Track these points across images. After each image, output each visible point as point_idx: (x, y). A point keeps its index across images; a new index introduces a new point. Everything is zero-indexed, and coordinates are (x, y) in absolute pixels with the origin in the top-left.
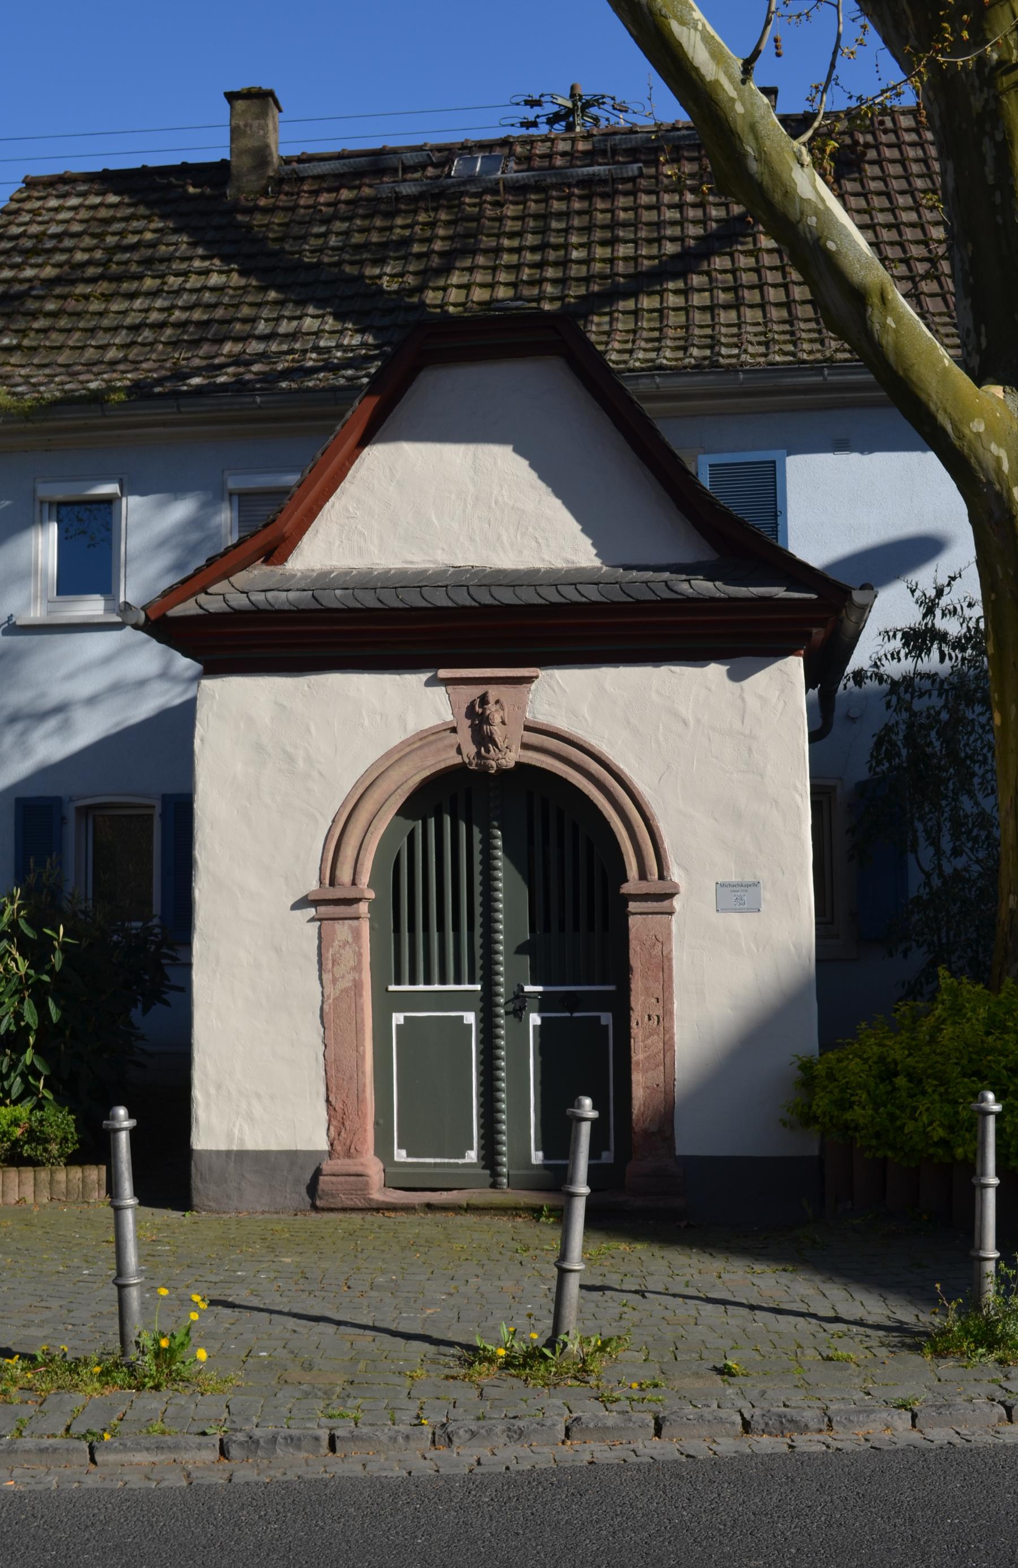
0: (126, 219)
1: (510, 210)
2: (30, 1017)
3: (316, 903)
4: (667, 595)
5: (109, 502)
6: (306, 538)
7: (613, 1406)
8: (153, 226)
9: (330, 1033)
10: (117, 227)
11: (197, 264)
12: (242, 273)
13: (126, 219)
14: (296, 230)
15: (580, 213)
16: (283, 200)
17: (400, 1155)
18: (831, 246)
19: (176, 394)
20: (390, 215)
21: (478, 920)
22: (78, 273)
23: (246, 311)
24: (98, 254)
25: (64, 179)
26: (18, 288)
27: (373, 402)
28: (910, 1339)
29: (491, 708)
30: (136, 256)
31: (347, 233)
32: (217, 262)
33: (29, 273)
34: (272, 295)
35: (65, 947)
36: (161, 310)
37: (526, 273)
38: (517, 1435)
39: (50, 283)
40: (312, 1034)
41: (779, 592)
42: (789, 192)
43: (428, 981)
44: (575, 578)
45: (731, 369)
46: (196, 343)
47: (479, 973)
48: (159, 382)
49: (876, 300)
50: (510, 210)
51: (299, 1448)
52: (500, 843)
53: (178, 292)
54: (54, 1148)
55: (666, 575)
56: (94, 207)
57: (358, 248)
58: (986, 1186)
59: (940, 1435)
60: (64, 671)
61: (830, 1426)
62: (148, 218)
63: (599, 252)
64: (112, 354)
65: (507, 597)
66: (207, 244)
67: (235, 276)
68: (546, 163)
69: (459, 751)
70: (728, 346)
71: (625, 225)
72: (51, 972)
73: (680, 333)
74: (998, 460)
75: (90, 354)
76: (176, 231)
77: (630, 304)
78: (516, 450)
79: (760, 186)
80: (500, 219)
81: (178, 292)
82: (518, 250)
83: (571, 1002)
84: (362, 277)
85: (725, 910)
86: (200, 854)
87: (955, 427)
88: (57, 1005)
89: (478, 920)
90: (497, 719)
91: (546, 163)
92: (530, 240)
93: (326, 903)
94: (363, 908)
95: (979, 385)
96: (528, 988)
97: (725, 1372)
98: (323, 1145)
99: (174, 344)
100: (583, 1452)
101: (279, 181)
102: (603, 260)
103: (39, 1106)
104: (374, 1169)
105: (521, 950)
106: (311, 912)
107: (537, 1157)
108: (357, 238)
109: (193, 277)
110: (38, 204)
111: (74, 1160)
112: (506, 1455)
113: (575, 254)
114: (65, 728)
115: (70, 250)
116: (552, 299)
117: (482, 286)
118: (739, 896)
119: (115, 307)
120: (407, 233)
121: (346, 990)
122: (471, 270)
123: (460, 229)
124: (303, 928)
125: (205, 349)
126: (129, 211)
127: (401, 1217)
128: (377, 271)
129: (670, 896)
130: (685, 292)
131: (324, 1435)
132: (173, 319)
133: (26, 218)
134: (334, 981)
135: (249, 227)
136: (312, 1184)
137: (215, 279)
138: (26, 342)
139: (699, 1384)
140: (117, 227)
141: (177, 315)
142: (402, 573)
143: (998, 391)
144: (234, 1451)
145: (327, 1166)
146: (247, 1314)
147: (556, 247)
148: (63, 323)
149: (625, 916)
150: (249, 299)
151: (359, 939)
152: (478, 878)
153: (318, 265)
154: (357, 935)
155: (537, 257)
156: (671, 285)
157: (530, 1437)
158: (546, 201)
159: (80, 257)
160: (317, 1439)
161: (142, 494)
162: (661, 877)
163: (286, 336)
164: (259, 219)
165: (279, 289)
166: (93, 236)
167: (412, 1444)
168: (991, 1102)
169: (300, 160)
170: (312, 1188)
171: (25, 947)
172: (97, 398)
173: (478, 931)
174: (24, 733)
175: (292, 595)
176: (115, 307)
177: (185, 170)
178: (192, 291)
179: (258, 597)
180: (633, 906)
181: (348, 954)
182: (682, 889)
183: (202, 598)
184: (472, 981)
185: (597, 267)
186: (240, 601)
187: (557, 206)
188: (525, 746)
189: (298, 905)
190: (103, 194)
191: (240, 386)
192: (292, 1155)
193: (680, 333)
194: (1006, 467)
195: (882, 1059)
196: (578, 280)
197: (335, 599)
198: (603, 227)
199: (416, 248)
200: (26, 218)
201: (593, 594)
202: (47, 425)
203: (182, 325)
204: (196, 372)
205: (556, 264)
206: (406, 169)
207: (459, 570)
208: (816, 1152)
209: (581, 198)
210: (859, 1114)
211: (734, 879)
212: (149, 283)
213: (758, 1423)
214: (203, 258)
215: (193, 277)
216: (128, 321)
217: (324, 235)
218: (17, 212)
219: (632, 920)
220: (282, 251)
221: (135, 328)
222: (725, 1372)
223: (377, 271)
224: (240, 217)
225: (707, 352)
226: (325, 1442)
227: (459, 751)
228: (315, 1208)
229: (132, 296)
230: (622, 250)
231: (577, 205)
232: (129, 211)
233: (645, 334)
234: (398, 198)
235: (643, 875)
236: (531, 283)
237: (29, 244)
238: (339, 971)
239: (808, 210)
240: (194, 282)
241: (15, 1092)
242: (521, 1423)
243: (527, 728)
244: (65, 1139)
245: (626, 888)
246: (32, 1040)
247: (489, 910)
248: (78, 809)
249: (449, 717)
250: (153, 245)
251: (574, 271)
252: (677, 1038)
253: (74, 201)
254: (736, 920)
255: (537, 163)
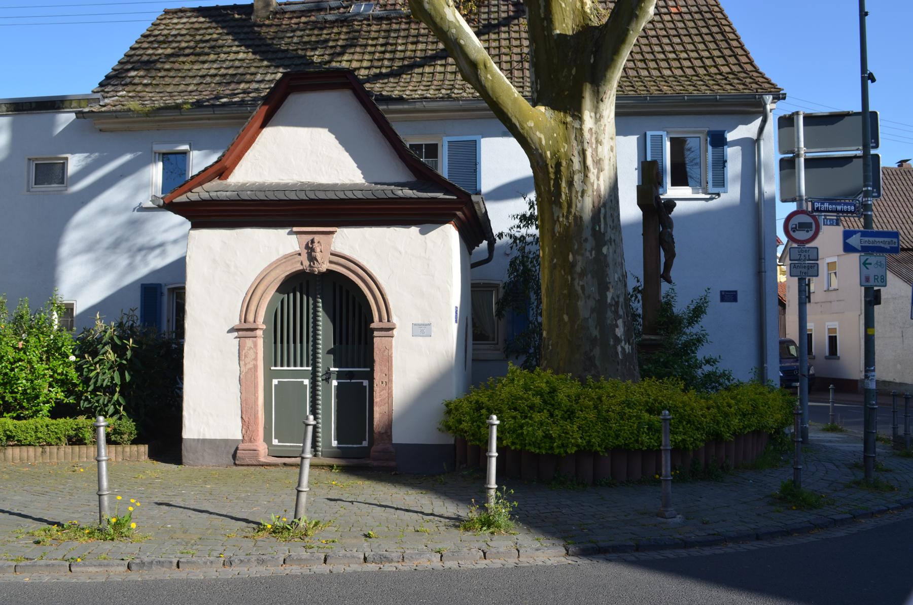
0: (206, 29)
1: (374, 28)
2: (117, 380)
3: (238, 330)
4: (391, 196)
5: (184, 153)
6: (237, 168)
7: (308, 550)
8: (217, 32)
9: (243, 388)
10: (202, 32)
11: (234, 49)
12: (254, 53)
13: (206, 29)
14: (280, 35)
15: (404, 30)
16: (276, 21)
17: (275, 442)
18: (462, 42)
19: (213, 106)
20: (321, 29)
21: (311, 339)
22: (182, 52)
23: (253, 70)
24: (192, 44)
25: (181, 11)
26: (154, 58)
27: (266, 108)
28: (458, 522)
29: (316, 245)
30: (208, 45)
31: (302, 37)
32: (243, 48)
33: (160, 51)
34: (265, 63)
35: (132, 349)
36: (216, 69)
37: (377, 56)
38: (261, 562)
39: (169, 56)
40: (235, 388)
41: (440, 195)
42: (443, 18)
43: (302, 365)
44: (353, 188)
45: (457, 99)
46: (229, 83)
47: (311, 362)
48: (208, 100)
49: (482, 67)
50: (374, 28)
51: (163, 566)
52: (321, 305)
53: (224, 61)
54: (126, 437)
55: (393, 187)
56: (193, 23)
57: (306, 43)
58: (491, 457)
59: (451, 564)
60: (163, 228)
61: (403, 560)
62: (216, 28)
63: (410, 47)
64: (191, 88)
65: (322, 196)
66: (240, 40)
67: (250, 54)
68: (392, 8)
69: (302, 264)
70: (458, 89)
71: (423, 35)
72: (126, 360)
73: (440, 83)
74: (540, 139)
75: (182, 87)
76: (227, 34)
77: (420, 70)
78: (330, 131)
79: (430, 14)
80: (369, 32)
81: (224, 61)
82: (375, 46)
83: (351, 375)
84: (305, 56)
85: (416, 336)
86: (188, 308)
87: (520, 124)
88: (129, 374)
89: (311, 339)
90: (318, 250)
91: (392, 8)
92: (381, 41)
93: (243, 330)
94: (259, 333)
95: (534, 106)
96: (332, 369)
97: (367, 536)
98: (240, 437)
99: (219, 84)
100: (294, 569)
101: (275, 13)
102: (412, 51)
103: (120, 419)
104: (262, 448)
105: (329, 352)
106: (236, 334)
107: (335, 443)
108: (306, 39)
109: (232, 55)
110: (168, 21)
111: (134, 442)
112: (256, 571)
113: (399, 48)
114: (163, 253)
115: (179, 42)
116: (387, 67)
117: (357, 61)
118: (422, 329)
119: (196, 67)
120: (328, 37)
121: (250, 369)
122: (353, 54)
123: (351, 36)
124: (232, 341)
125: (233, 86)
126: (208, 25)
127: (272, 469)
128: (312, 53)
129: (392, 329)
130: (444, 66)
131: (175, 561)
132: (220, 73)
133: (162, 27)
134: (245, 365)
135: (259, 33)
136: (234, 454)
137: (241, 56)
138: (154, 82)
139: (354, 541)
140: (202, 32)
141: (223, 71)
142: (278, 185)
143: (542, 109)
144: (133, 567)
145: (240, 447)
146: (174, 509)
147: (392, 45)
148: (172, 74)
149: (372, 338)
150: (255, 64)
151: (259, 345)
152: (311, 320)
153: (287, 50)
154: (255, 345)
155: (383, 49)
156: (439, 62)
157: (277, 562)
158: (390, 24)
159: (184, 45)
160: (171, 562)
161: (199, 150)
162: (388, 321)
163: (269, 81)
164: (264, 29)
165: (269, 60)
166: (191, 35)
167: (214, 565)
168: (495, 419)
169: (285, 4)
170: (234, 456)
171: (115, 348)
172: (178, 107)
173: (311, 343)
174: (145, 255)
175: (228, 193)
176: (196, 67)
177: (235, 8)
178: (231, 61)
179: (213, 194)
180: (376, 334)
181: (251, 353)
182: (398, 326)
183: (189, 194)
184: (308, 366)
185: (408, 54)
186: (205, 196)
187: (395, 26)
188: (331, 262)
189: (232, 330)
190: (198, 17)
191: (242, 103)
192: (226, 442)
193: (440, 83)
194: (544, 142)
195: (477, 402)
196: (399, 59)
197: (246, 196)
198: (414, 36)
199: (331, 44)
200: (162, 27)
201: (359, 195)
202: (157, 118)
203: (224, 75)
204: (226, 96)
205: (391, 52)
206: (331, 9)
207: (303, 184)
208: (453, 442)
209: (406, 23)
210: (464, 425)
211: (420, 322)
212: (212, 57)
213: (370, 559)
214: (237, 46)
215: (232, 55)
216: (201, 73)
217: (292, 37)
218: (158, 25)
219: (375, 339)
220: (273, 44)
221: (203, 77)
222: (367, 536)
223: (312, 53)
224: (256, 29)
225: (449, 92)
226: (175, 564)
227: (302, 264)
228: (235, 464)
229: (204, 62)
230: (420, 46)
231: (403, 26)
232: (208, 25)
233: (424, 83)
234: (326, 21)
235: (381, 320)
236: (379, 60)
237: (161, 38)
238: (248, 360)
239: (451, 25)
240: (232, 56)
241: (110, 412)
242: (264, 557)
243: (332, 254)
244: (131, 433)
245: (373, 326)
246: (118, 389)
247: (315, 334)
248: (169, 289)
249: (298, 249)
250: (216, 40)
251: (398, 55)
252: (394, 392)
253: (184, 20)
254: (420, 340)
255: (389, 7)
